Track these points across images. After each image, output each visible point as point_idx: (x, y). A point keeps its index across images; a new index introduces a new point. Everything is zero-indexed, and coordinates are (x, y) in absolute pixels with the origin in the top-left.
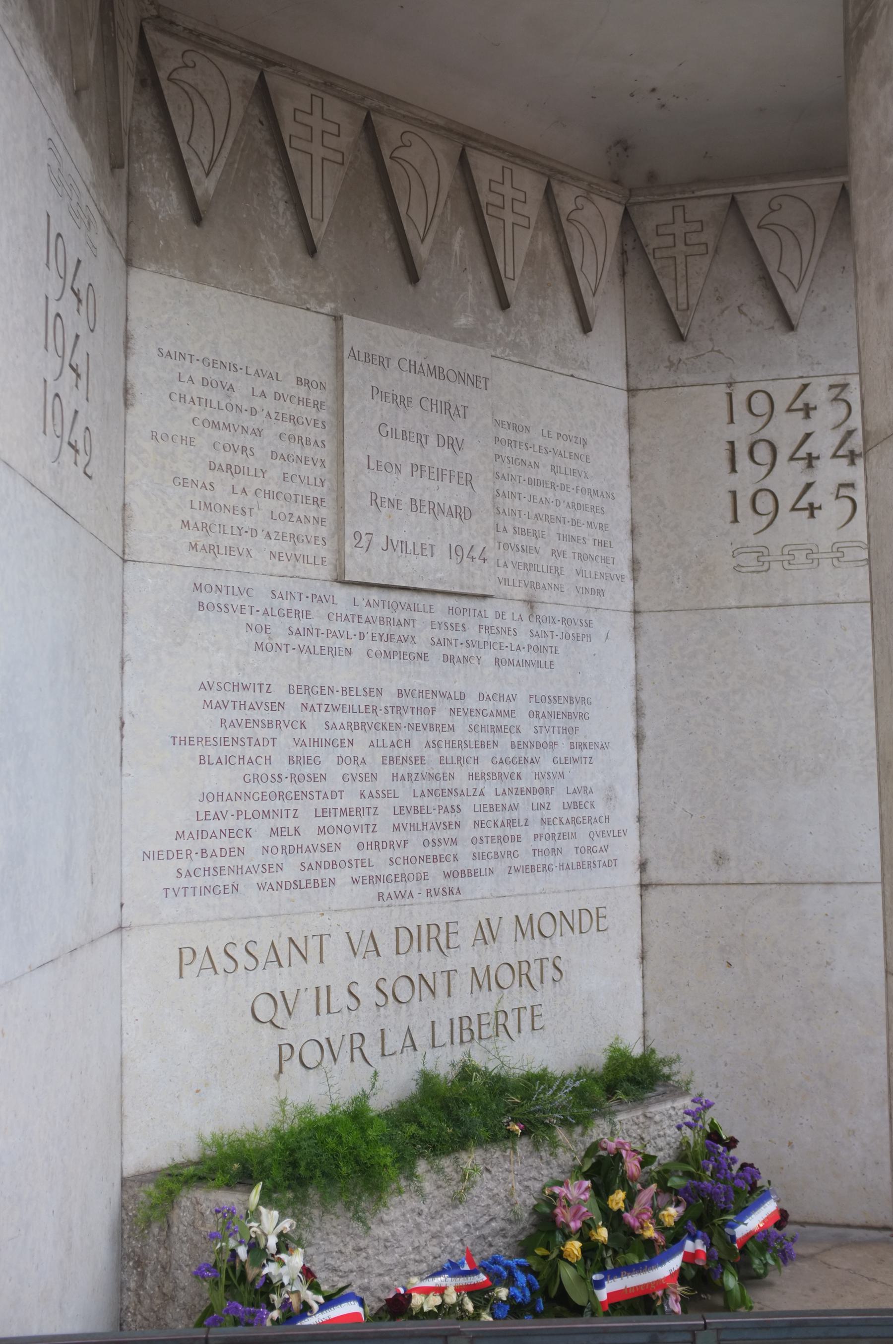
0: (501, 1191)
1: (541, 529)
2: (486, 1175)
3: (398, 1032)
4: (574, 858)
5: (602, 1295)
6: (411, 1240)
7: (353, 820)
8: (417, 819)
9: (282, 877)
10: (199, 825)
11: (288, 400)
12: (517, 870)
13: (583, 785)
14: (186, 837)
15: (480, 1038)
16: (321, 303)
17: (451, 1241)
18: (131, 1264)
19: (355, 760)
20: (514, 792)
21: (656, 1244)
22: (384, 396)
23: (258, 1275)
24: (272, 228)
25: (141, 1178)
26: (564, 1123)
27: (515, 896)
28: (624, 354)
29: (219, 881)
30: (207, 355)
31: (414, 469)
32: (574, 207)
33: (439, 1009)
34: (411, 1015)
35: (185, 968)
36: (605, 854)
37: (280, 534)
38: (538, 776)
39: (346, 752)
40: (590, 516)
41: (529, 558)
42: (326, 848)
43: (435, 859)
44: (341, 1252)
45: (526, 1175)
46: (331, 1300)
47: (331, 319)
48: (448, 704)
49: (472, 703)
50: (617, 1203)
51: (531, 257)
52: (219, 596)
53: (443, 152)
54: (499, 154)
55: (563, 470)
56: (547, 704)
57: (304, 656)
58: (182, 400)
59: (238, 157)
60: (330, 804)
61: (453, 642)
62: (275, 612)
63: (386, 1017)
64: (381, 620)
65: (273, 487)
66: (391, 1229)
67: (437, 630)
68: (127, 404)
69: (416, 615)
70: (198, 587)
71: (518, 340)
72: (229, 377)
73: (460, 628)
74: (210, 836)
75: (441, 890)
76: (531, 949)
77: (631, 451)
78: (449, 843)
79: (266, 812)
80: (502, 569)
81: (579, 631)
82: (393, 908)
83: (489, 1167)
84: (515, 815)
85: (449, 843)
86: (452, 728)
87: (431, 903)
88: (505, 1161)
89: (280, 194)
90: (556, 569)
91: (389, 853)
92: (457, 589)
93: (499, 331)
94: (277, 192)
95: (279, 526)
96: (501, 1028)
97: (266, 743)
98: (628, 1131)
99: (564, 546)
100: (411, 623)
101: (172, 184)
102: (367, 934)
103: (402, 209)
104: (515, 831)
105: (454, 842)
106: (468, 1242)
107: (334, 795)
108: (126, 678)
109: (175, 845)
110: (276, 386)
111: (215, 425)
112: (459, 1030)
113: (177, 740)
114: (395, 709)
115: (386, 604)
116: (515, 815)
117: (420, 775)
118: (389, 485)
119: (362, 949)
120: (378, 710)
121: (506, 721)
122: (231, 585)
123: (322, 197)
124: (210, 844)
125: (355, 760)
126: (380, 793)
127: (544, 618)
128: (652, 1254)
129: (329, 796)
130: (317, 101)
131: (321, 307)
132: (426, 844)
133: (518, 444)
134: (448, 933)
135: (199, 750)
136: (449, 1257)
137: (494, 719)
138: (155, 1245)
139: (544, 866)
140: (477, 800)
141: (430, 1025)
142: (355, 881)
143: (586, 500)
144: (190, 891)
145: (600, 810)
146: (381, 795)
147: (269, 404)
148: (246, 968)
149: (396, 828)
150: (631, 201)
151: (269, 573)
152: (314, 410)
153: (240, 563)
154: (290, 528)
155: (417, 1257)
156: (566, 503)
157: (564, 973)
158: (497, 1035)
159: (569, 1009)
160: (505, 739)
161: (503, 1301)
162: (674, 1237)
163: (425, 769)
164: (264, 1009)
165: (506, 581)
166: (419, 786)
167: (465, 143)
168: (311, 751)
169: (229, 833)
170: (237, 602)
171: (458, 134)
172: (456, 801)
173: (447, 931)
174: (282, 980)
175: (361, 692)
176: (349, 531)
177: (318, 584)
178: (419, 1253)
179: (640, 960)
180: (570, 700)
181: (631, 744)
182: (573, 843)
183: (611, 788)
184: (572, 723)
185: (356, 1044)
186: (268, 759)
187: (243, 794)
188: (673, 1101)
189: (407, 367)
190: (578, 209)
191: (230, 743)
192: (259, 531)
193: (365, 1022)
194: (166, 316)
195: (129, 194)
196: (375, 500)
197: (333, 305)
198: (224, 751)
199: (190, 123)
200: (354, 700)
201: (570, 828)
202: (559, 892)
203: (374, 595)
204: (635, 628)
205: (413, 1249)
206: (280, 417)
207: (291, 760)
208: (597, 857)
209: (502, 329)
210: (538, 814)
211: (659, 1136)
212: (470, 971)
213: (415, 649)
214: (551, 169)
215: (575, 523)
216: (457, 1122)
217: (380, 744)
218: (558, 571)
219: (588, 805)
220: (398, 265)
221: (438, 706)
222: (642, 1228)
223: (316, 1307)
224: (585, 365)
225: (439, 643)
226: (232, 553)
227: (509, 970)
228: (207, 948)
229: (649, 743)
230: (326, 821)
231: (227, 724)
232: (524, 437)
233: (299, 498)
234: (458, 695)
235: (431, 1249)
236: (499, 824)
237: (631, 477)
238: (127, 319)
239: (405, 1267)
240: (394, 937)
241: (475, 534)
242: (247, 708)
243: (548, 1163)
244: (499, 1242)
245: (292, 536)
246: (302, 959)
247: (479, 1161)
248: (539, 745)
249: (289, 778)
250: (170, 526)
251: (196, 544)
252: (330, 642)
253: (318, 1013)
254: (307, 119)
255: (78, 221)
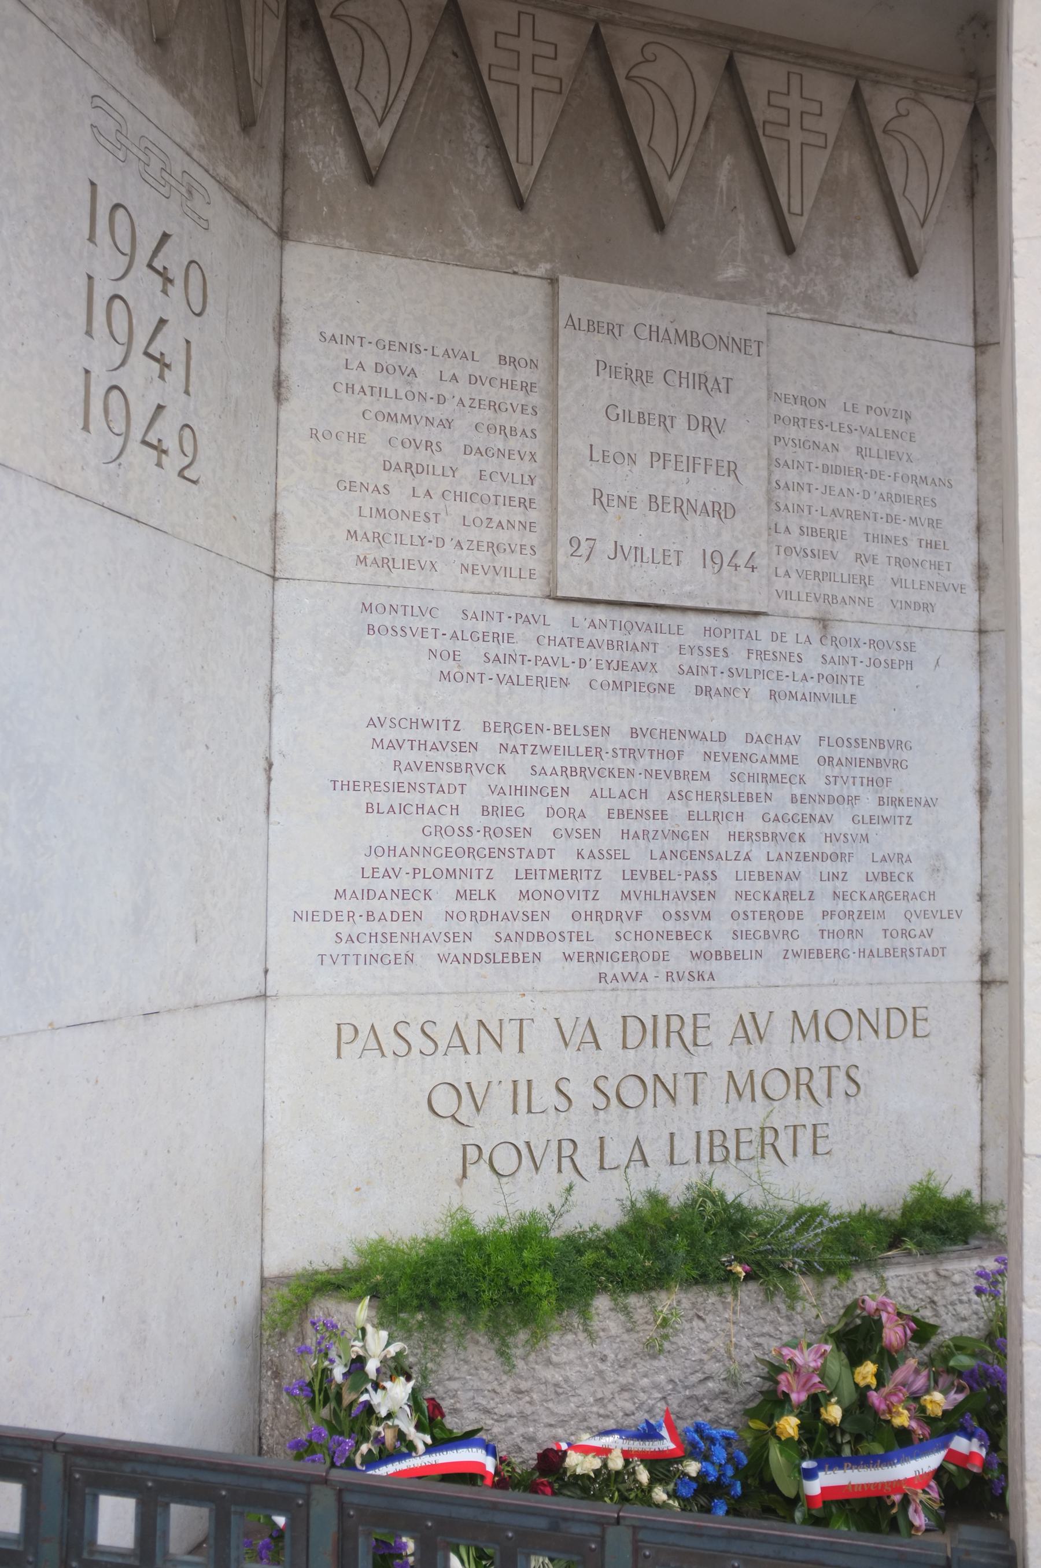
0: (718, 1343)
1: (840, 528)
2: (696, 1323)
3: (623, 1142)
4: (882, 943)
5: (813, 1488)
6: (592, 1390)
7: (568, 885)
8: (656, 886)
9: (470, 948)
10: (364, 884)
11: (487, 384)
12: (796, 955)
13: (898, 850)
14: (348, 897)
15: (738, 1158)
16: (533, 264)
17: (649, 1398)
18: (269, 1373)
19: (571, 813)
20: (794, 857)
21: (914, 1436)
22: (614, 372)
23: (355, 1400)
24: (468, 180)
25: (282, 1280)
26: (808, 1269)
27: (793, 986)
28: (971, 299)
29: (389, 949)
30: (381, 336)
31: (655, 459)
32: (894, 114)
33: (680, 1119)
34: (641, 1123)
35: (343, 1047)
36: (928, 939)
37: (475, 543)
38: (829, 838)
39: (559, 802)
40: (914, 510)
41: (819, 565)
42: (531, 917)
43: (679, 935)
44: (494, 1391)
45: (756, 1330)
46: (442, 1442)
47: (545, 283)
48: (701, 747)
49: (736, 745)
50: (864, 1378)
51: (828, 186)
52: (394, 617)
53: (702, 65)
54: (782, 57)
55: (874, 453)
56: (845, 748)
57: (505, 688)
58: (350, 391)
59: (424, 100)
60: (536, 864)
61: (711, 670)
62: (467, 636)
63: (607, 1123)
64: (610, 644)
65: (466, 488)
66: (563, 1372)
67: (688, 656)
68: (279, 399)
69: (659, 638)
70: (367, 608)
71: (810, 292)
72: (410, 360)
73: (721, 653)
74: (378, 896)
75: (687, 974)
76: (815, 1054)
77: (978, 425)
78: (699, 917)
79: (451, 871)
80: (783, 580)
81: (893, 655)
82: (619, 992)
83: (701, 1314)
84: (794, 885)
85: (699, 917)
86: (707, 777)
87: (671, 989)
88: (725, 1308)
89: (479, 138)
90: (862, 578)
91: (615, 925)
92: (713, 605)
93: (783, 282)
94: (476, 136)
95: (474, 534)
96: (768, 1149)
97: (452, 790)
98: (910, 1290)
99: (874, 549)
100: (651, 647)
101: (339, 139)
102: (584, 1021)
103: (642, 141)
104: (795, 906)
105: (707, 916)
106: (674, 1403)
107: (541, 853)
108: (276, 712)
109: (334, 906)
110: (470, 367)
111: (392, 417)
112: (708, 1147)
113: (338, 785)
114: (627, 752)
115: (617, 624)
116: (794, 885)
117: (660, 832)
118: (616, 480)
119: (576, 1039)
120: (603, 754)
121: (784, 769)
122: (410, 604)
123: (530, 136)
124: (377, 906)
125: (571, 813)
126: (604, 853)
127: (843, 640)
128: (904, 1443)
129: (535, 854)
130: (526, 20)
131: (534, 269)
132: (667, 916)
133: (808, 423)
134: (695, 1027)
135: (366, 796)
136: (647, 1416)
137: (768, 765)
138: (291, 1357)
139: (836, 952)
140: (741, 866)
141: (668, 1137)
142: (568, 958)
143: (910, 489)
144: (352, 959)
145: (921, 884)
146: (606, 855)
147: (463, 390)
148: (421, 1052)
149: (626, 896)
150: (981, 95)
151: (459, 589)
152: (522, 394)
153: (421, 578)
154: (487, 536)
155: (602, 1411)
156: (878, 495)
157: (862, 1087)
158: (763, 1157)
159: (869, 1132)
160: (782, 792)
161: (690, 1478)
162: (943, 1428)
163: (668, 826)
164: (445, 1102)
165: (788, 595)
166: (657, 846)
167: (732, 49)
168: (511, 801)
169: (403, 894)
170: (417, 624)
171: (719, 37)
172: (710, 866)
173: (695, 1024)
174: (469, 1070)
175: (580, 730)
176: (563, 537)
177: (524, 601)
178: (605, 1406)
179: (978, 1077)
180: (881, 744)
181: (971, 802)
182: (879, 924)
183: (939, 856)
184: (882, 773)
185: (566, 1152)
186: (455, 810)
187: (421, 849)
188: (982, 1259)
189: (646, 334)
190: (900, 115)
191: (406, 788)
192: (447, 540)
193: (578, 1125)
194: (331, 294)
195: (285, 156)
196: (599, 498)
197: (548, 266)
198: (397, 798)
199: (358, 65)
200: (572, 741)
201: (877, 905)
202: (857, 984)
203: (600, 614)
204: (980, 653)
205: (596, 1400)
206: (476, 404)
207: (484, 810)
208: (915, 943)
209: (788, 278)
210: (829, 886)
211: (961, 1302)
212: (726, 1076)
213: (656, 679)
214: (857, 67)
215: (891, 519)
216: (658, 1254)
217: (606, 793)
218: (865, 581)
219: (904, 877)
220: (640, 211)
221: (686, 749)
222: (890, 1412)
223: (421, 1448)
224: (911, 318)
225: (690, 671)
226: (412, 567)
227: (782, 1077)
228: (373, 1026)
229: (993, 801)
230: (531, 885)
231: (403, 767)
232: (818, 413)
233: (501, 500)
234: (716, 736)
235: (621, 1404)
236: (772, 896)
237: (978, 458)
238: (281, 301)
239: (585, 1420)
240: (620, 1028)
241: (741, 536)
242: (429, 748)
243: (789, 1318)
244: (720, 1408)
245: (491, 545)
246: (495, 1046)
247: (686, 1304)
248: (832, 800)
249: (482, 832)
250: (332, 537)
251: (365, 558)
252: (540, 670)
253: (515, 1112)
254: (512, 43)
255: (162, 189)
